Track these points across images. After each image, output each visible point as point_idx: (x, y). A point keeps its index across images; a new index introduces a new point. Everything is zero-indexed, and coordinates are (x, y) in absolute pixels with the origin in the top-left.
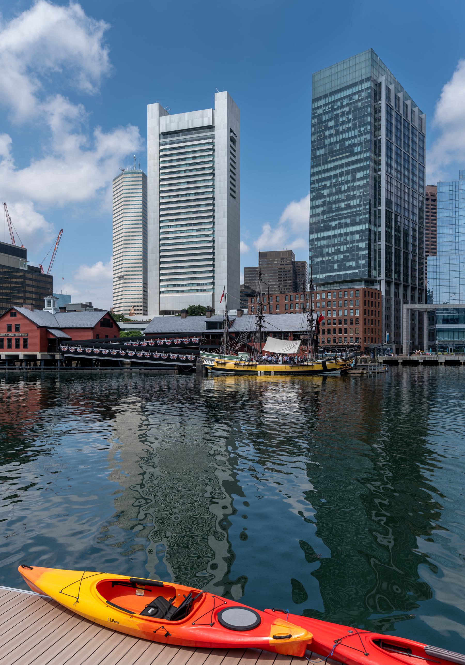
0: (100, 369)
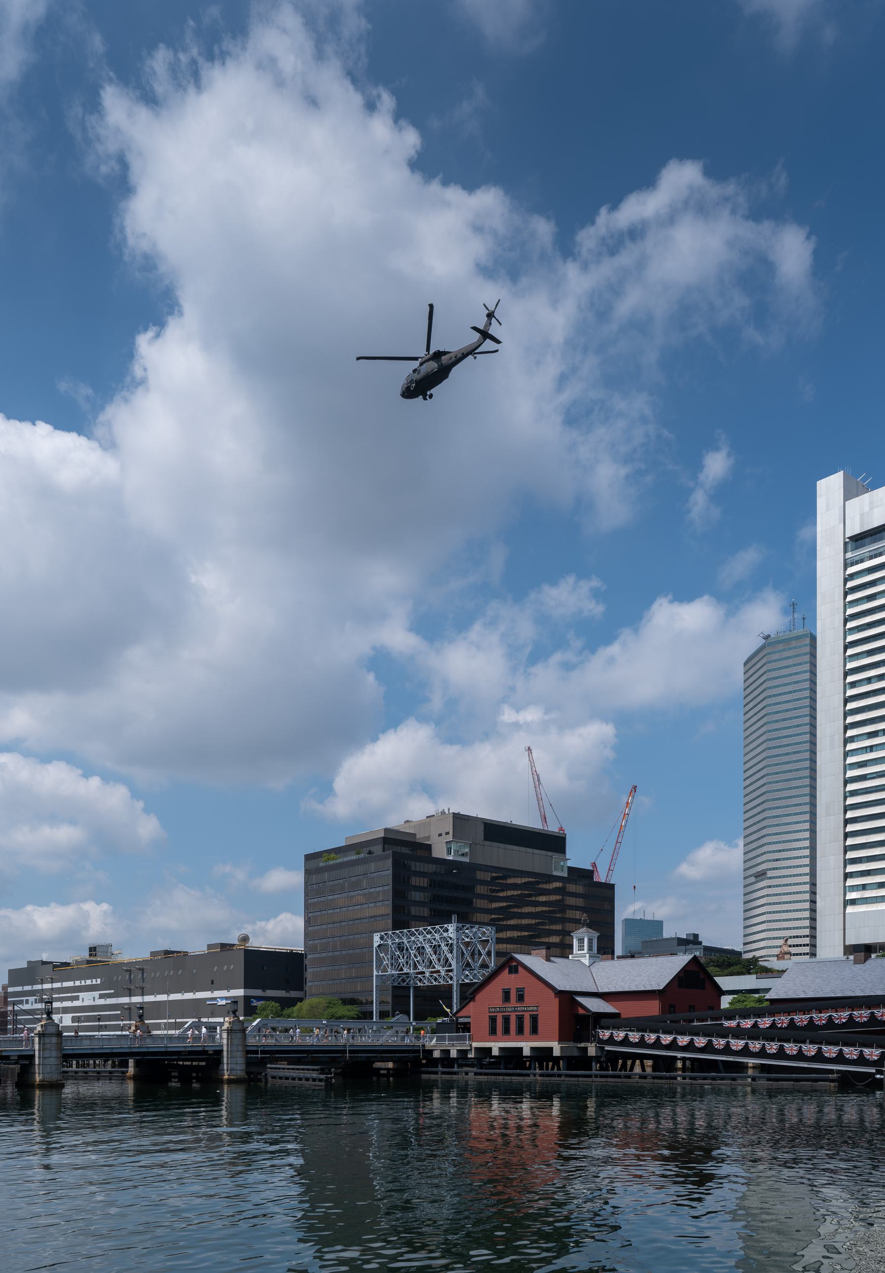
0: (476, 1074)
